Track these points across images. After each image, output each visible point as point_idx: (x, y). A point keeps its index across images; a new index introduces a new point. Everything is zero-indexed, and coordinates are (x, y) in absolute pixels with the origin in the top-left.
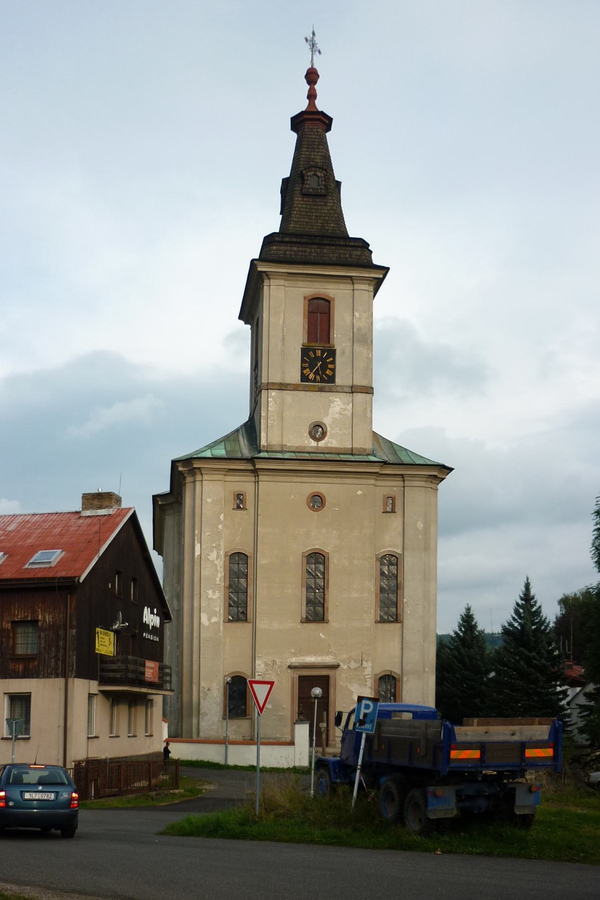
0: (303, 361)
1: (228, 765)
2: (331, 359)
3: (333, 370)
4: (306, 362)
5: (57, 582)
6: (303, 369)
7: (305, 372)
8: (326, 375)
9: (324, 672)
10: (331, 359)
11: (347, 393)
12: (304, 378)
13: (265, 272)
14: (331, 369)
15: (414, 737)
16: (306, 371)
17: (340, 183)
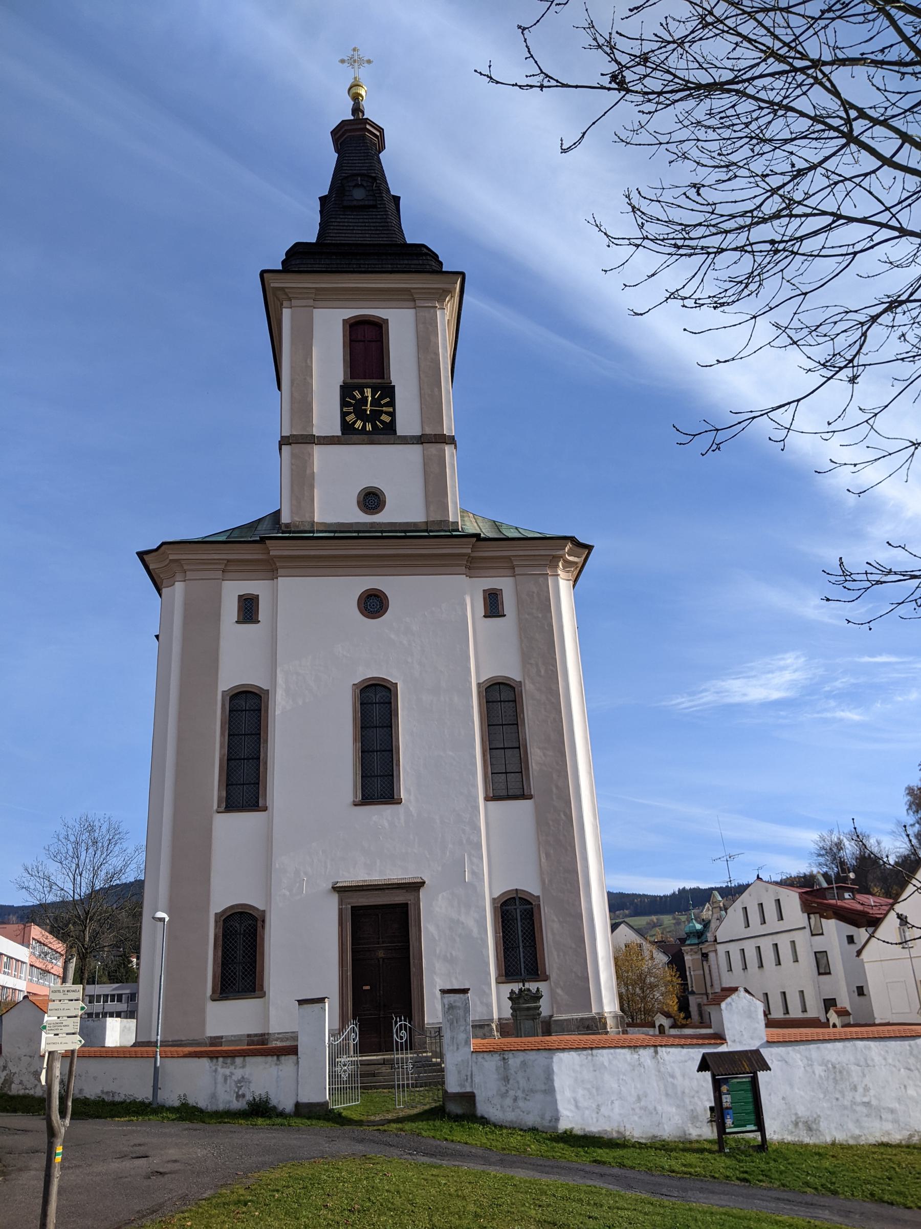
0: (344, 403)
1: (512, 1015)
2: (388, 399)
3: (392, 415)
4: (349, 404)
5: (836, 887)
6: (344, 415)
7: (348, 419)
8: (382, 422)
9: (398, 898)
10: (388, 399)
11: (910, 1006)
12: (347, 428)
13: (283, 289)
14: (387, 413)
15: (364, 1058)
16: (350, 418)
17: (399, 197)
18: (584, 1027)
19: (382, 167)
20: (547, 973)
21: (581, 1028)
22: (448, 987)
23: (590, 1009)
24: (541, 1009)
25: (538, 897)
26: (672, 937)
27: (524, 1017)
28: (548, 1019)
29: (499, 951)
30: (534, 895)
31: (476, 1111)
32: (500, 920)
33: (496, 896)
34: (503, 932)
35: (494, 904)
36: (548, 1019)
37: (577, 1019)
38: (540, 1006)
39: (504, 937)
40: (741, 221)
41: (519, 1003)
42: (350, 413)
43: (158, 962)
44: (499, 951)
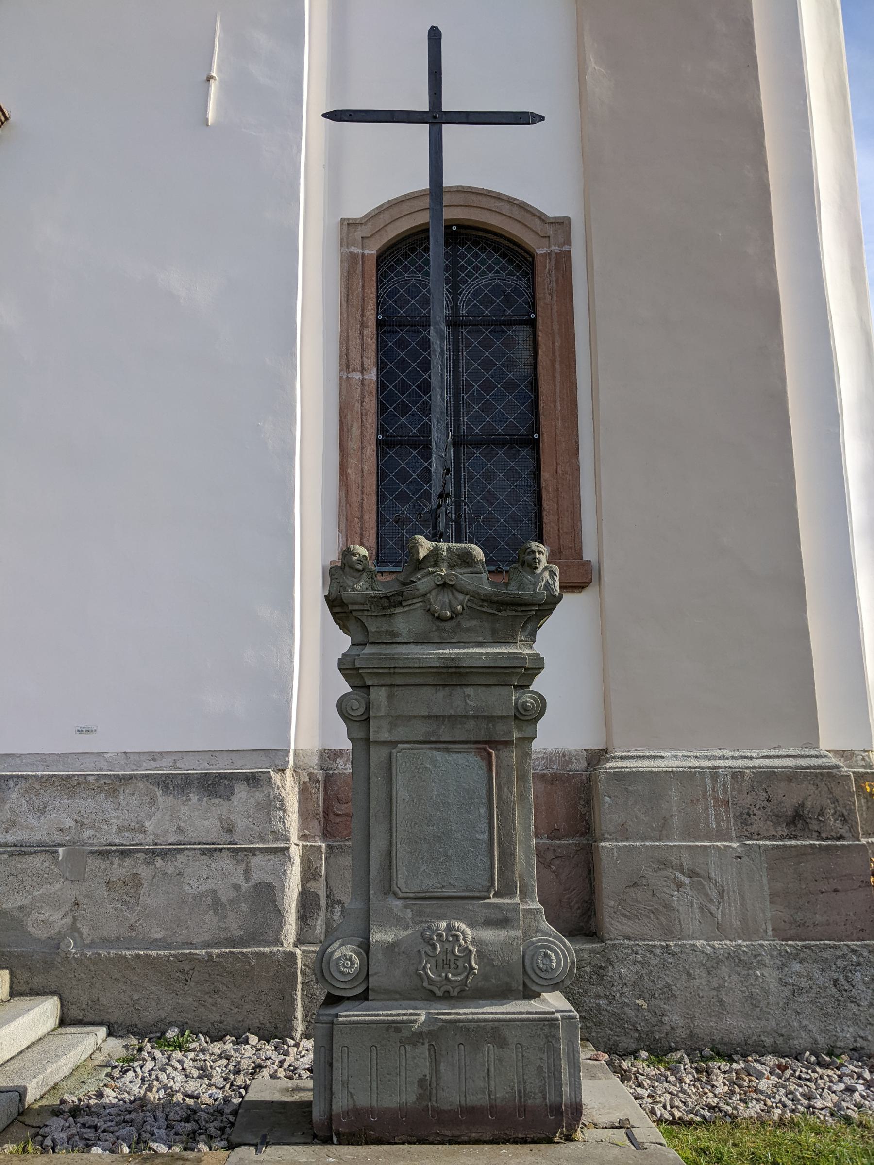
18: (777, 818)
20: (589, 554)
21: (758, 824)
23: (814, 742)
24: (537, 685)
25: (563, 224)
26: (93, 928)
27: (419, 730)
28: (580, 765)
29: (353, 445)
30: (542, 217)
32: (371, 316)
33: (358, 210)
34: (381, 366)
35: (344, 242)
36: (580, 765)
37: (736, 775)
38: (536, 667)
39: (381, 386)
40: (432, 1053)
41: (392, 639)
44: (353, 445)
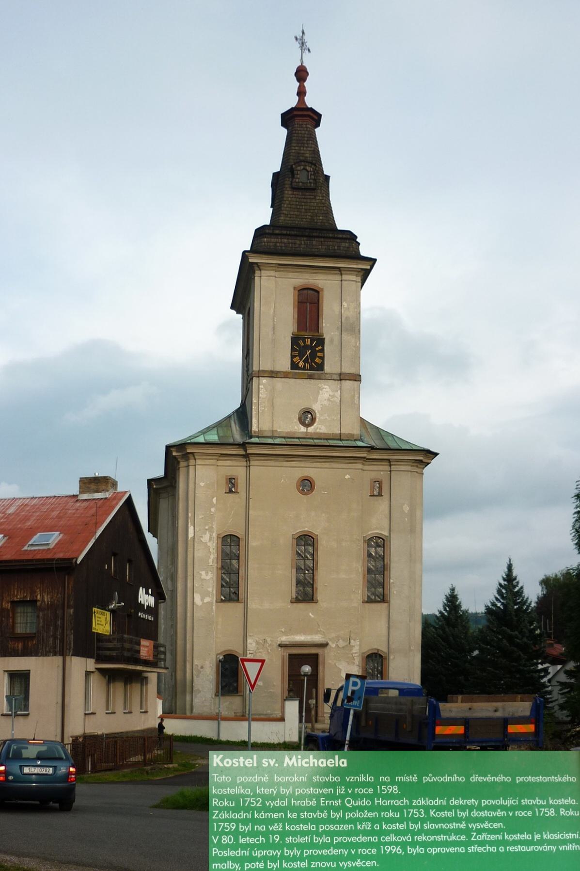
0: (293, 350)
2: (320, 347)
3: (322, 358)
4: (296, 350)
6: (293, 357)
7: (294, 360)
8: (316, 363)
10: (320, 347)
12: (294, 366)
13: (256, 263)
19: (330, 204)
22: (140, 706)
31: (461, 734)
42: (296, 356)
43: (66, 584)
